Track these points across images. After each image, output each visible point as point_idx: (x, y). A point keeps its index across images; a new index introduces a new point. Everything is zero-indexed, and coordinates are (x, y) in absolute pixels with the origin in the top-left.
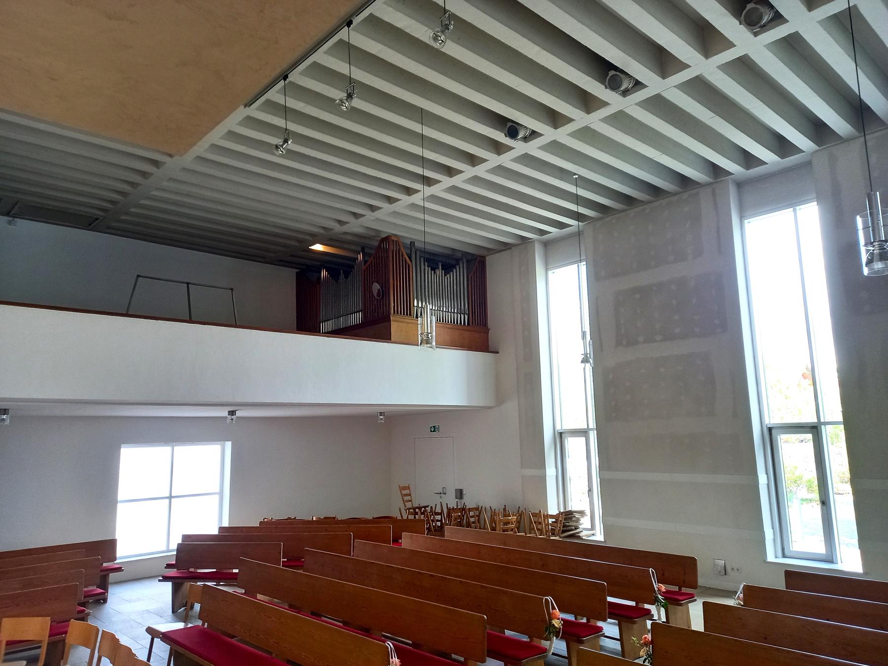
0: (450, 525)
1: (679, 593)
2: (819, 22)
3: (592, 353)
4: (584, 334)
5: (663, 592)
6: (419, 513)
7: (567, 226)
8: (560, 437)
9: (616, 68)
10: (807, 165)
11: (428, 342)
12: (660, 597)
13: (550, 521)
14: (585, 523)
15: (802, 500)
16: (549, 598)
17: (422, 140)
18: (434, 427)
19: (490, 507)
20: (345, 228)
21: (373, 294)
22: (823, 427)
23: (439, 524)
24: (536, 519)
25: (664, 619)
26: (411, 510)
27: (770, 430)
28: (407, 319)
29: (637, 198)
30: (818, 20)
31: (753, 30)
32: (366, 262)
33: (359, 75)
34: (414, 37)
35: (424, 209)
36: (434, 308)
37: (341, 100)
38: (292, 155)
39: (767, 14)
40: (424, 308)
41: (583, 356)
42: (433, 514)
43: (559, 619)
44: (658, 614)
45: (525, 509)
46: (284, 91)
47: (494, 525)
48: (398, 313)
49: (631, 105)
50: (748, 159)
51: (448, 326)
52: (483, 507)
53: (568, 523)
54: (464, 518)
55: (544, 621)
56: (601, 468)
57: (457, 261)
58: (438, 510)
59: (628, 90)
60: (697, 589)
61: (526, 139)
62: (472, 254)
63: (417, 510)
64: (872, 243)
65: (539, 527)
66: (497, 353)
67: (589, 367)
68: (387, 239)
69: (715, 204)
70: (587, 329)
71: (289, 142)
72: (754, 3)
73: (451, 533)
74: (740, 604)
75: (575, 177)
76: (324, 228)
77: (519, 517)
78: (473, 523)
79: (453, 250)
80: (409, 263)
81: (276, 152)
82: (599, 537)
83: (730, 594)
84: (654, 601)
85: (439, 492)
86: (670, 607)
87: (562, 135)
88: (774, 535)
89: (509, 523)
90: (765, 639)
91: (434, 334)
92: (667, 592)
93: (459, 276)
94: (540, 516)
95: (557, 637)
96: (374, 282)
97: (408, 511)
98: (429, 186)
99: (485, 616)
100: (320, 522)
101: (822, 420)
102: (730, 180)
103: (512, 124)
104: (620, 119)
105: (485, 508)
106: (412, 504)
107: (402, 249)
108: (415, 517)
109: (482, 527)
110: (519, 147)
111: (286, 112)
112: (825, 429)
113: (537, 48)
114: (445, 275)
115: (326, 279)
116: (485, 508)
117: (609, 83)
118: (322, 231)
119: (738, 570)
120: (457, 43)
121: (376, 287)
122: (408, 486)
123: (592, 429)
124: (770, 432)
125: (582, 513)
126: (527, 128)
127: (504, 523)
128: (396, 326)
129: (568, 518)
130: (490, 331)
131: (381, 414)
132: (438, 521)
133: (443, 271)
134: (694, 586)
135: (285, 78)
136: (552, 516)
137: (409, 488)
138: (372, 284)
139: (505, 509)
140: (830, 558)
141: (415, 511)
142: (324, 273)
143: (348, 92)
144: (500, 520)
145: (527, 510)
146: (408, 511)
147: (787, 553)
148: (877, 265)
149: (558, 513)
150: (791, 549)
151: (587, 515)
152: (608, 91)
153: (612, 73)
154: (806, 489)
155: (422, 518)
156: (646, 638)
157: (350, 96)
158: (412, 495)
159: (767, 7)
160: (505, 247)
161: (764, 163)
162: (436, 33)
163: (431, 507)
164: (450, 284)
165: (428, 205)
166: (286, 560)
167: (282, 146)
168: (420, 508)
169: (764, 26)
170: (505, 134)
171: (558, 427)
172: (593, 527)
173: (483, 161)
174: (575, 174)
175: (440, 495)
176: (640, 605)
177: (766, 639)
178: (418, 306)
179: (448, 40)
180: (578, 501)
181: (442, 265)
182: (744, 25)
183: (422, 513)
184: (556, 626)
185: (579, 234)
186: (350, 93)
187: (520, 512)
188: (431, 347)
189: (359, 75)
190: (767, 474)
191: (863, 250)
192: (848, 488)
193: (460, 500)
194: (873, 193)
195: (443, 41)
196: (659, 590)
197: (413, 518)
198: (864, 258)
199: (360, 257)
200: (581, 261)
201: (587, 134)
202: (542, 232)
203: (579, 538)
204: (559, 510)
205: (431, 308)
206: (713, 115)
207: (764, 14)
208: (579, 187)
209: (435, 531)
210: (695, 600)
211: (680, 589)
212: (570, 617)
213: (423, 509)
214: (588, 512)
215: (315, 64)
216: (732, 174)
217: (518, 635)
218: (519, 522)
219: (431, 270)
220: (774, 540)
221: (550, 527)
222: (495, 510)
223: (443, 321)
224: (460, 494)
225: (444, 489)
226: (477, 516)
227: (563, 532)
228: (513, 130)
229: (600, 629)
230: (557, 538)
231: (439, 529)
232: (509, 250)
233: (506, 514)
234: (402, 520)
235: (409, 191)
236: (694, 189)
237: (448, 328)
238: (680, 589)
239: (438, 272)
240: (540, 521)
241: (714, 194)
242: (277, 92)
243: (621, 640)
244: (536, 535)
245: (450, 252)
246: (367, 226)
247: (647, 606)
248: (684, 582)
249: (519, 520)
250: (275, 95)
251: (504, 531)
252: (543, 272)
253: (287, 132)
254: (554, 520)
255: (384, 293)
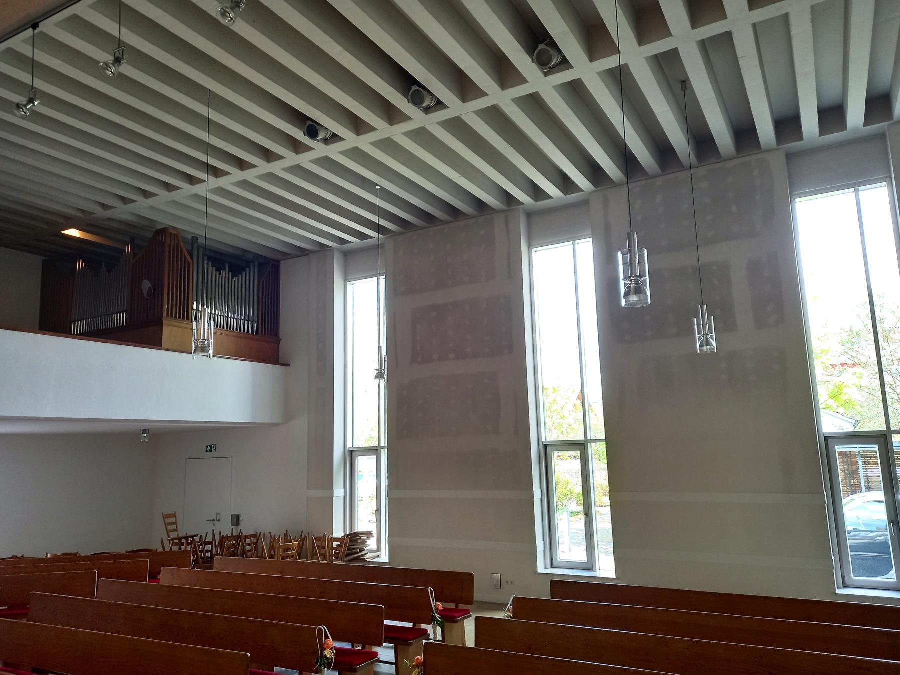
0: (222, 556)
1: (456, 610)
2: (598, 73)
3: (386, 370)
4: (380, 348)
5: (441, 611)
6: (186, 544)
7: (369, 237)
8: (351, 456)
9: (419, 84)
10: (584, 204)
11: (204, 350)
12: (437, 615)
13: (335, 544)
14: (372, 544)
15: (572, 512)
16: (323, 628)
17: (209, 125)
18: (211, 446)
19: (270, 533)
20: (109, 214)
21: (142, 291)
22: (589, 444)
23: (208, 555)
24: (320, 544)
25: (440, 638)
26: (175, 541)
27: (546, 446)
28: (184, 324)
29: (437, 216)
30: (598, 71)
31: (543, 70)
32: (135, 255)
33: (131, 38)
34: (202, 10)
35: (207, 201)
36: (217, 314)
37: (106, 64)
38: (36, 117)
39: (555, 57)
40: (201, 312)
41: (377, 372)
42: (202, 544)
43: (332, 649)
44: (434, 633)
45: (309, 533)
46: (33, 42)
47: (273, 553)
48: (172, 316)
49: (432, 123)
50: (537, 192)
51: (241, 335)
52: (262, 535)
53: (353, 545)
54: (239, 547)
55: (315, 652)
56: (390, 487)
57: (248, 263)
58: (209, 539)
59: (430, 108)
60: (473, 606)
61: (326, 141)
62: (265, 257)
63: (183, 541)
64: (629, 278)
65: (323, 552)
66: (289, 365)
67: (383, 384)
68: (163, 231)
69: (508, 232)
70: (383, 344)
71: (36, 103)
72: (545, 45)
73: (221, 565)
74: (509, 616)
75: (377, 188)
76: (83, 211)
77: (302, 543)
78: (249, 551)
79: (244, 251)
80: (190, 262)
81: (16, 112)
82: (384, 558)
83: (501, 607)
84: (431, 620)
85: (212, 519)
86: (447, 625)
87: (364, 143)
88: (545, 548)
89: (290, 549)
90: (529, 649)
91: (212, 341)
92: (445, 609)
93: (249, 280)
94: (325, 540)
95: (329, 668)
96: (145, 279)
97: (172, 542)
98: (217, 177)
99: (249, 654)
100: (56, 559)
101: (589, 438)
102: (521, 210)
103: (311, 123)
104: (422, 136)
105: (264, 534)
106: (178, 534)
107: (182, 244)
108: (180, 549)
109: (259, 555)
110: (319, 149)
111: (33, 66)
112: (591, 446)
113: (339, 49)
114: (233, 278)
115: (82, 270)
116: (264, 534)
117: (412, 97)
118: (79, 215)
119: (512, 583)
120: (252, 26)
121: (146, 285)
122: (174, 513)
123: (383, 447)
124: (546, 449)
125: (369, 534)
126: (328, 130)
127: (284, 550)
128: (169, 331)
129: (354, 540)
130: (281, 342)
131: (145, 431)
132: (207, 551)
133: (231, 273)
134: (470, 602)
135: (35, 26)
136: (337, 540)
137: (174, 516)
138: (142, 282)
139: (286, 535)
140: (590, 566)
141: (180, 542)
142: (80, 264)
143: (116, 56)
144: (280, 547)
145: (310, 534)
146: (172, 542)
147: (555, 564)
148: (633, 297)
149: (343, 535)
150: (559, 560)
151: (374, 536)
152: (411, 105)
153: (415, 88)
154: (576, 502)
155: (189, 549)
156: (418, 659)
157: (118, 61)
158: (178, 524)
159: (556, 51)
160: (302, 253)
161: (552, 198)
162: (224, 9)
163: (201, 536)
164: (229, 289)
165: (212, 197)
166: (6, 608)
167: (26, 106)
168: (187, 538)
169: (553, 68)
170: (304, 133)
171: (349, 445)
172: (379, 549)
173: (280, 158)
174: (378, 185)
175: (212, 522)
176: (418, 626)
177: (530, 649)
178: (197, 310)
179: (238, 18)
180: (365, 522)
181: (230, 267)
182: (536, 64)
183: (189, 544)
184: (328, 656)
185: (379, 247)
186: (119, 57)
187: (303, 537)
188: (207, 356)
189: (131, 38)
190: (541, 489)
191: (622, 283)
192: (607, 500)
193: (236, 527)
194: (632, 233)
195: (232, 19)
196: (437, 609)
197: (178, 550)
198: (623, 290)
199: (129, 249)
200: (379, 275)
201: (388, 145)
202: (342, 241)
203: (364, 561)
204: (344, 532)
205: (210, 312)
206: (508, 146)
207: (553, 57)
208: (206, 142)
209: (204, 563)
210: (471, 616)
211: (457, 607)
212: (347, 646)
213: (191, 539)
214: (375, 534)
215: (75, 18)
216: (524, 204)
217: (285, 671)
218: (300, 548)
219: (216, 271)
220: (545, 551)
221: (334, 551)
222: (275, 535)
223: (227, 328)
224: (236, 520)
225: (218, 515)
226: (254, 544)
227: (348, 555)
228: (313, 130)
229: (376, 654)
230: (341, 563)
231: (208, 561)
232: (306, 257)
233: (287, 539)
234: (165, 553)
235: (192, 180)
236: (489, 214)
237: (232, 336)
238: (457, 607)
239: (224, 273)
240: (324, 545)
241: (507, 223)
242: (23, 41)
243: (396, 664)
244: (319, 561)
245: (239, 253)
246: (138, 213)
247: (424, 626)
248: (461, 599)
249: (301, 545)
250: (20, 43)
251: (283, 558)
252: (342, 283)
253: (34, 91)
254: (339, 543)
255: (156, 293)
